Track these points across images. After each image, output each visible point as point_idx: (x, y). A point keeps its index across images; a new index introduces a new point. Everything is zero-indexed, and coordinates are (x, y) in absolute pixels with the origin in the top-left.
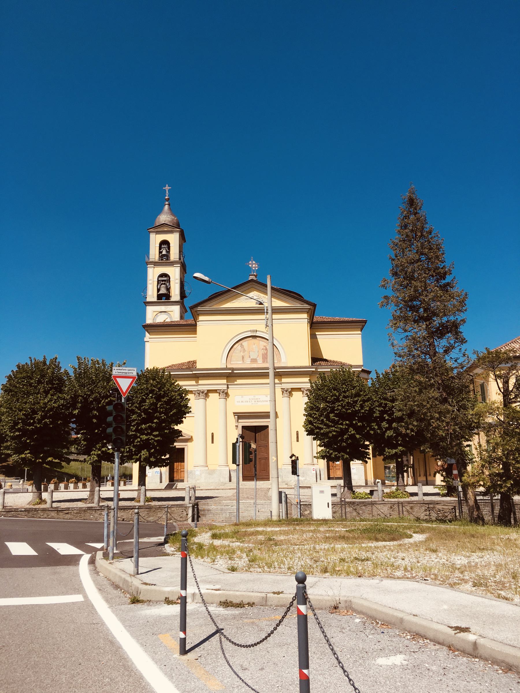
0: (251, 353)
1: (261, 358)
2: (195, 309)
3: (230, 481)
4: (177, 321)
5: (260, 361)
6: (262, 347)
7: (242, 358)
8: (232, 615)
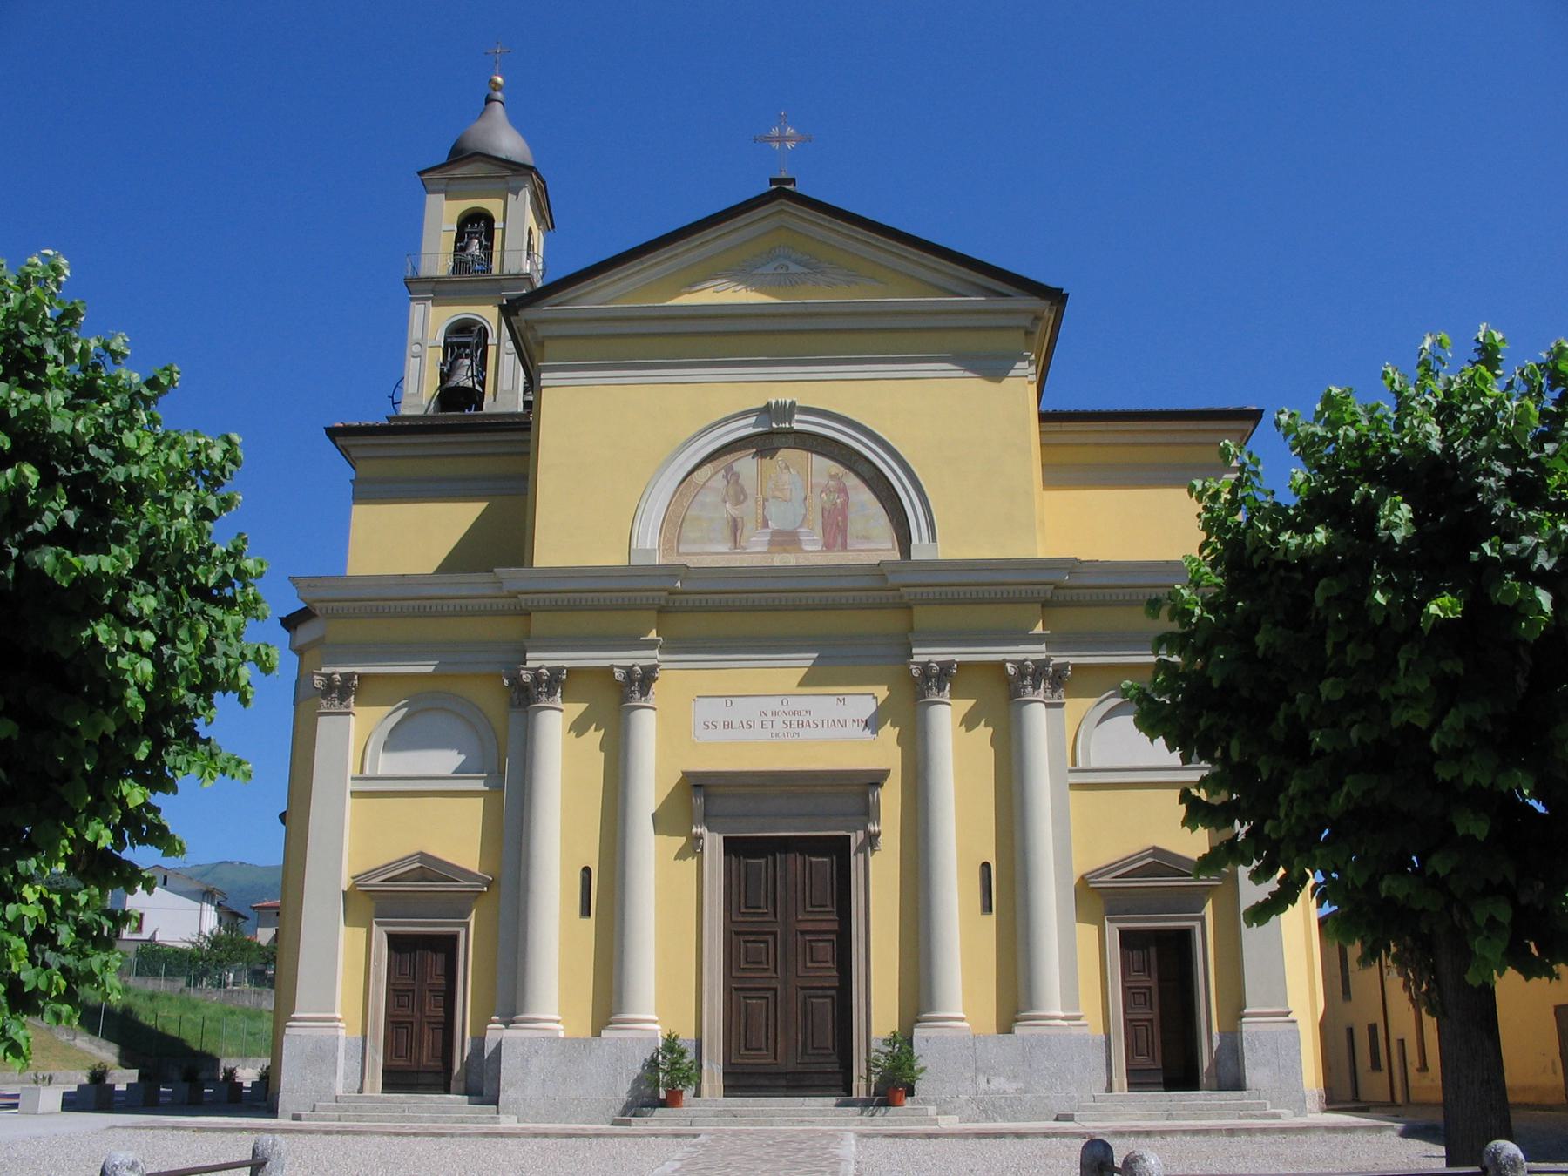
0: (773, 509)
1: (819, 529)
2: (527, 314)
7: (727, 533)
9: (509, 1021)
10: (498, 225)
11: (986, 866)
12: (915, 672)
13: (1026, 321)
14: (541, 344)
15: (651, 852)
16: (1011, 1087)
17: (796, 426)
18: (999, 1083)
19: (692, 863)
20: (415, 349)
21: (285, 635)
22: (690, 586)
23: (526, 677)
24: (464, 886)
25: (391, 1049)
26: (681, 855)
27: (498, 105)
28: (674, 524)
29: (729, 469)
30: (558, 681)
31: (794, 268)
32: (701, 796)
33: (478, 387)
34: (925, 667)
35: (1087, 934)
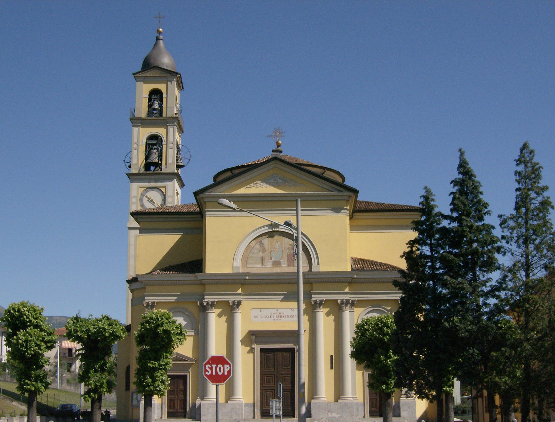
0: (273, 254)
1: (286, 260)
2: (201, 195)
3: (254, 418)
4: (177, 206)
5: (284, 264)
6: (287, 246)
7: (260, 261)
8: (442, 399)
9: (202, 399)
10: (164, 95)
11: (332, 356)
12: (313, 303)
13: (347, 198)
14: (205, 203)
15: (240, 351)
16: (337, 416)
17: (280, 230)
18: (334, 415)
19: (251, 355)
20: (135, 146)
21: (128, 285)
22: (250, 278)
23: (205, 304)
24: (189, 362)
25: (169, 406)
26: (249, 352)
27: (161, 41)
28: (246, 259)
29: (261, 242)
30: (214, 305)
31: (279, 181)
32: (254, 337)
33: (160, 162)
34: (316, 301)
35: (359, 374)
